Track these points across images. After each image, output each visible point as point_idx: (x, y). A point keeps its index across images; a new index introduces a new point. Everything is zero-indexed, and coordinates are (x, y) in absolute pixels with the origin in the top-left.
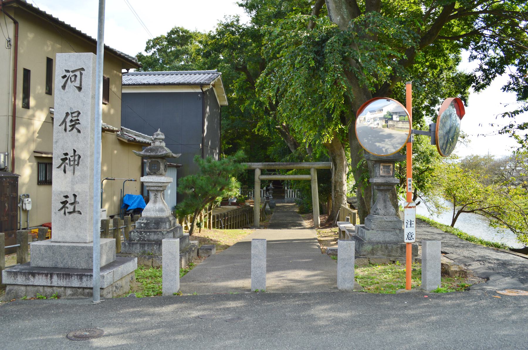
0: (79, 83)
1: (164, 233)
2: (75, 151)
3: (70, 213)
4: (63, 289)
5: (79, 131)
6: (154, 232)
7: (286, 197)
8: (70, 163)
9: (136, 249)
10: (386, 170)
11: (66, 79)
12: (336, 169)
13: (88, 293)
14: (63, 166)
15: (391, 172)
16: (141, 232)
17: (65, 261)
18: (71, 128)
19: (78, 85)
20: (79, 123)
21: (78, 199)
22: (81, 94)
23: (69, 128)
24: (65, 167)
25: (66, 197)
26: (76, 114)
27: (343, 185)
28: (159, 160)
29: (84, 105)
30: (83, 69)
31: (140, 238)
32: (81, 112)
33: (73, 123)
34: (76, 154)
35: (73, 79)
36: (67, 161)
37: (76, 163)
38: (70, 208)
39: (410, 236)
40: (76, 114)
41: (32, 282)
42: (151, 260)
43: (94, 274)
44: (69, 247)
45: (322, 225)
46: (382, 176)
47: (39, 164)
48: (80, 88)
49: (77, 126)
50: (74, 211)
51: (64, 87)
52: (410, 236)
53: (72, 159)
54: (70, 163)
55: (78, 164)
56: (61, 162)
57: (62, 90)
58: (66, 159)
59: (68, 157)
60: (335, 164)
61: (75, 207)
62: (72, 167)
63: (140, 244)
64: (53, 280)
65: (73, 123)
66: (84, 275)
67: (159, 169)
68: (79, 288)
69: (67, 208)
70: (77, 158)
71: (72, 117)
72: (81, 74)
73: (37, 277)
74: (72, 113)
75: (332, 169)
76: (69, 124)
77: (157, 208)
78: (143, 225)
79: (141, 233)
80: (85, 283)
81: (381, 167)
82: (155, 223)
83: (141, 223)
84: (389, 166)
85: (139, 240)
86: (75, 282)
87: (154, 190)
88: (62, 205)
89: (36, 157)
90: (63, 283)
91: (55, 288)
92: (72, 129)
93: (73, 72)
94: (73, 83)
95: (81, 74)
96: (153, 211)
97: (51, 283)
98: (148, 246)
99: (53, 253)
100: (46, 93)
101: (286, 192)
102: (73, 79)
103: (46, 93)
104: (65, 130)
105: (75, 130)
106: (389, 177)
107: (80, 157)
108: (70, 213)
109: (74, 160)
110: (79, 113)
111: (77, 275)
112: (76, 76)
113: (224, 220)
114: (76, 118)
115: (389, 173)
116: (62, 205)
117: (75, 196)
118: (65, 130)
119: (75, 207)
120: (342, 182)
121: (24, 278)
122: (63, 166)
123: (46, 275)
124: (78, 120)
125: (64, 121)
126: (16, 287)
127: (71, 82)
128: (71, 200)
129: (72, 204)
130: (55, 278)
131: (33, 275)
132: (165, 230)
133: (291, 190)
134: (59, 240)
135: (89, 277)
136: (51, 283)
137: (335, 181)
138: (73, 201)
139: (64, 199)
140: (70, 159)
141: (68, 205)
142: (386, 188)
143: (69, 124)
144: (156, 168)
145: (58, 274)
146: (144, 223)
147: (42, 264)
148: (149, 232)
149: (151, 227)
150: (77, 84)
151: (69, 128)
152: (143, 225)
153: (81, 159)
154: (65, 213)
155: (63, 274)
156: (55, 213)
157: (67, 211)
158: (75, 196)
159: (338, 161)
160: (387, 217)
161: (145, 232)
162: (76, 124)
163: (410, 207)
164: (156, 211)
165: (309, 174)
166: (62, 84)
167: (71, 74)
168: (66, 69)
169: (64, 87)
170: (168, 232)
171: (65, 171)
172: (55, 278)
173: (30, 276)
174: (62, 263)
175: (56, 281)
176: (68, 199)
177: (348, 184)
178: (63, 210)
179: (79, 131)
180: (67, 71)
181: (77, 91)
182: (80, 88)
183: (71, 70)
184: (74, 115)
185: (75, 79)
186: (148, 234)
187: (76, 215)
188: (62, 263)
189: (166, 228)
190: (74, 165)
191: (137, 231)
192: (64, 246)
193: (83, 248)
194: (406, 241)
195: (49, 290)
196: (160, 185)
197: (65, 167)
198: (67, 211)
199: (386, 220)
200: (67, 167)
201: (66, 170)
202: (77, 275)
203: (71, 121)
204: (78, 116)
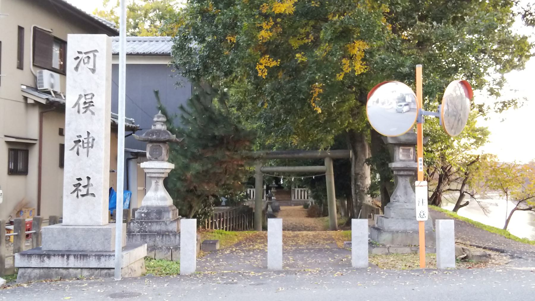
0: (93, 64)
1: (168, 223)
2: (88, 133)
3: (83, 196)
4: (79, 270)
5: (93, 113)
6: (157, 222)
7: (293, 199)
8: (83, 145)
9: (136, 240)
10: (406, 153)
11: (78, 60)
12: (356, 159)
13: (106, 273)
14: (76, 149)
15: (412, 156)
16: (142, 222)
17: (79, 244)
18: (84, 110)
19: (92, 67)
20: (93, 105)
21: (91, 181)
22: (95, 76)
23: (82, 110)
24: (78, 150)
25: (79, 179)
26: (89, 97)
27: (366, 178)
28: (161, 145)
29: (98, 87)
30: (96, 51)
31: (141, 229)
32: (95, 94)
33: (87, 105)
34: (90, 136)
35: (86, 60)
36: (81, 143)
37: (90, 145)
38: (84, 191)
39: (422, 214)
40: (89, 97)
41: (47, 264)
42: (153, 252)
43: (116, 253)
44: (83, 229)
45: (340, 225)
46: (401, 160)
47: (10, 150)
48: (93, 71)
49: (91, 108)
50: (87, 194)
51: (76, 68)
52: (422, 214)
53: (85, 141)
54: (83, 145)
55: (92, 147)
56: (74, 144)
57: (75, 71)
58: (80, 141)
59: (81, 139)
60: (355, 153)
61: (88, 190)
62: (86, 149)
63: (141, 235)
64: (70, 261)
65: (87, 105)
66: (103, 255)
67: (161, 154)
68: (96, 269)
69: (80, 190)
70: (91, 140)
71: (86, 99)
72: (95, 56)
73: (53, 258)
74: (85, 95)
75: (352, 159)
76: (82, 106)
77: (159, 196)
78: (143, 215)
79: (141, 223)
80: (104, 263)
81: (401, 150)
82: (156, 213)
83: (141, 213)
84: (409, 150)
85: (139, 232)
86: (93, 263)
87: (155, 177)
88: (74, 188)
89: (7, 142)
90: (80, 264)
91: (71, 270)
92: (85, 112)
93: (85, 53)
94: (87, 65)
95: (95, 56)
96: (155, 199)
97: (68, 265)
98: (150, 237)
99: (67, 236)
100: (18, 68)
101: (292, 192)
102: (86, 60)
103: (18, 68)
104: (79, 112)
105: (88, 112)
106: (410, 161)
107: (94, 140)
108: (83, 196)
109: (88, 143)
110: (93, 95)
111: (95, 255)
112: (89, 57)
113: (220, 221)
114: (90, 100)
115: (409, 156)
116: (74, 188)
117: (89, 178)
118: (79, 112)
119: (88, 190)
120: (364, 174)
121: (39, 260)
122: (76, 149)
123: (63, 256)
124: (92, 102)
125: (77, 104)
126: (29, 270)
127: (84, 63)
128: (84, 182)
129: (85, 187)
130: (72, 258)
131: (49, 256)
132: (168, 220)
133: (300, 189)
134: (71, 224)
135: (107, 257)
136: (68, 265)
137: (355, 174)
138: (86, 184)
139: (78, 182)
140: (83, 141)
141: (81, 188)
142: (406, 173)
143: (82, 106)
144: (157, 153)
145: (75, 256)
146: (145, 213)
147: (54, 247)
148: (151, 222)
149: (152, 217)
150: (91, 65)
151: (82, 110)
152: (143, 215)
153: (95, 141)
154: (77, 196)
155: (81, 255)
156: (67, 196)
157: (80, 193)
158: (89, 178)
159: (359, 149)
160: (408, 204)
161: (146, 222)
162: (90, 105)
163: (421, 186)
164: (158, 200)
165: (323, 164)
166: (75, 66)
167: (85, 56)
168: (79, 51)
169: (76, 68)
170: (172, 222)
171: (78, 154)
172: (72, 258)
173: (45, 258)
174: (76, 246)
175: (73, 262)
176: (80, 182)
177: (368, 177)
178: (76, 193)
179: (93, 113)
180: (79, 53)
181: (90, 73)
182: (93, 71)
183: (83, 51)
184: (87, 97)
185: (88, 62)
186: (150, 224)
187: (89, 197)
188: (76, 246)
189: (169, 218)
190: (88, 147)
191: (137, 222)
192: (79, 229)
193: (99, 230)
194: (418, 219)
195: (64, 272)
196: (162, 171)
197: (78, 150)
198: (80, 193)
199: (407, 207)
200: (81, 149)
201: (80, 152)
202: (95, 255)
203: (85, 103)
204: (92, 98)
